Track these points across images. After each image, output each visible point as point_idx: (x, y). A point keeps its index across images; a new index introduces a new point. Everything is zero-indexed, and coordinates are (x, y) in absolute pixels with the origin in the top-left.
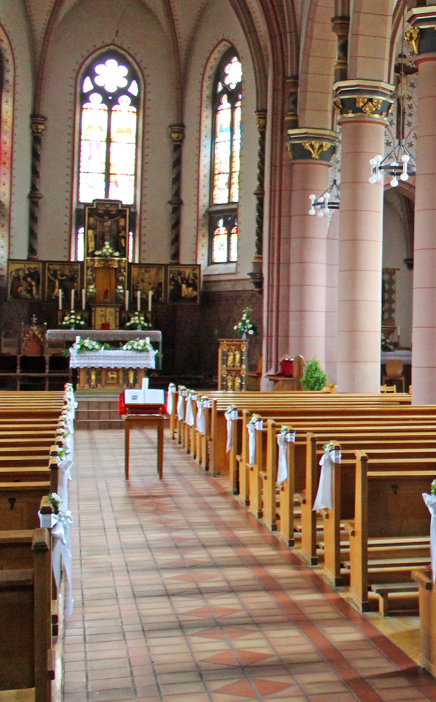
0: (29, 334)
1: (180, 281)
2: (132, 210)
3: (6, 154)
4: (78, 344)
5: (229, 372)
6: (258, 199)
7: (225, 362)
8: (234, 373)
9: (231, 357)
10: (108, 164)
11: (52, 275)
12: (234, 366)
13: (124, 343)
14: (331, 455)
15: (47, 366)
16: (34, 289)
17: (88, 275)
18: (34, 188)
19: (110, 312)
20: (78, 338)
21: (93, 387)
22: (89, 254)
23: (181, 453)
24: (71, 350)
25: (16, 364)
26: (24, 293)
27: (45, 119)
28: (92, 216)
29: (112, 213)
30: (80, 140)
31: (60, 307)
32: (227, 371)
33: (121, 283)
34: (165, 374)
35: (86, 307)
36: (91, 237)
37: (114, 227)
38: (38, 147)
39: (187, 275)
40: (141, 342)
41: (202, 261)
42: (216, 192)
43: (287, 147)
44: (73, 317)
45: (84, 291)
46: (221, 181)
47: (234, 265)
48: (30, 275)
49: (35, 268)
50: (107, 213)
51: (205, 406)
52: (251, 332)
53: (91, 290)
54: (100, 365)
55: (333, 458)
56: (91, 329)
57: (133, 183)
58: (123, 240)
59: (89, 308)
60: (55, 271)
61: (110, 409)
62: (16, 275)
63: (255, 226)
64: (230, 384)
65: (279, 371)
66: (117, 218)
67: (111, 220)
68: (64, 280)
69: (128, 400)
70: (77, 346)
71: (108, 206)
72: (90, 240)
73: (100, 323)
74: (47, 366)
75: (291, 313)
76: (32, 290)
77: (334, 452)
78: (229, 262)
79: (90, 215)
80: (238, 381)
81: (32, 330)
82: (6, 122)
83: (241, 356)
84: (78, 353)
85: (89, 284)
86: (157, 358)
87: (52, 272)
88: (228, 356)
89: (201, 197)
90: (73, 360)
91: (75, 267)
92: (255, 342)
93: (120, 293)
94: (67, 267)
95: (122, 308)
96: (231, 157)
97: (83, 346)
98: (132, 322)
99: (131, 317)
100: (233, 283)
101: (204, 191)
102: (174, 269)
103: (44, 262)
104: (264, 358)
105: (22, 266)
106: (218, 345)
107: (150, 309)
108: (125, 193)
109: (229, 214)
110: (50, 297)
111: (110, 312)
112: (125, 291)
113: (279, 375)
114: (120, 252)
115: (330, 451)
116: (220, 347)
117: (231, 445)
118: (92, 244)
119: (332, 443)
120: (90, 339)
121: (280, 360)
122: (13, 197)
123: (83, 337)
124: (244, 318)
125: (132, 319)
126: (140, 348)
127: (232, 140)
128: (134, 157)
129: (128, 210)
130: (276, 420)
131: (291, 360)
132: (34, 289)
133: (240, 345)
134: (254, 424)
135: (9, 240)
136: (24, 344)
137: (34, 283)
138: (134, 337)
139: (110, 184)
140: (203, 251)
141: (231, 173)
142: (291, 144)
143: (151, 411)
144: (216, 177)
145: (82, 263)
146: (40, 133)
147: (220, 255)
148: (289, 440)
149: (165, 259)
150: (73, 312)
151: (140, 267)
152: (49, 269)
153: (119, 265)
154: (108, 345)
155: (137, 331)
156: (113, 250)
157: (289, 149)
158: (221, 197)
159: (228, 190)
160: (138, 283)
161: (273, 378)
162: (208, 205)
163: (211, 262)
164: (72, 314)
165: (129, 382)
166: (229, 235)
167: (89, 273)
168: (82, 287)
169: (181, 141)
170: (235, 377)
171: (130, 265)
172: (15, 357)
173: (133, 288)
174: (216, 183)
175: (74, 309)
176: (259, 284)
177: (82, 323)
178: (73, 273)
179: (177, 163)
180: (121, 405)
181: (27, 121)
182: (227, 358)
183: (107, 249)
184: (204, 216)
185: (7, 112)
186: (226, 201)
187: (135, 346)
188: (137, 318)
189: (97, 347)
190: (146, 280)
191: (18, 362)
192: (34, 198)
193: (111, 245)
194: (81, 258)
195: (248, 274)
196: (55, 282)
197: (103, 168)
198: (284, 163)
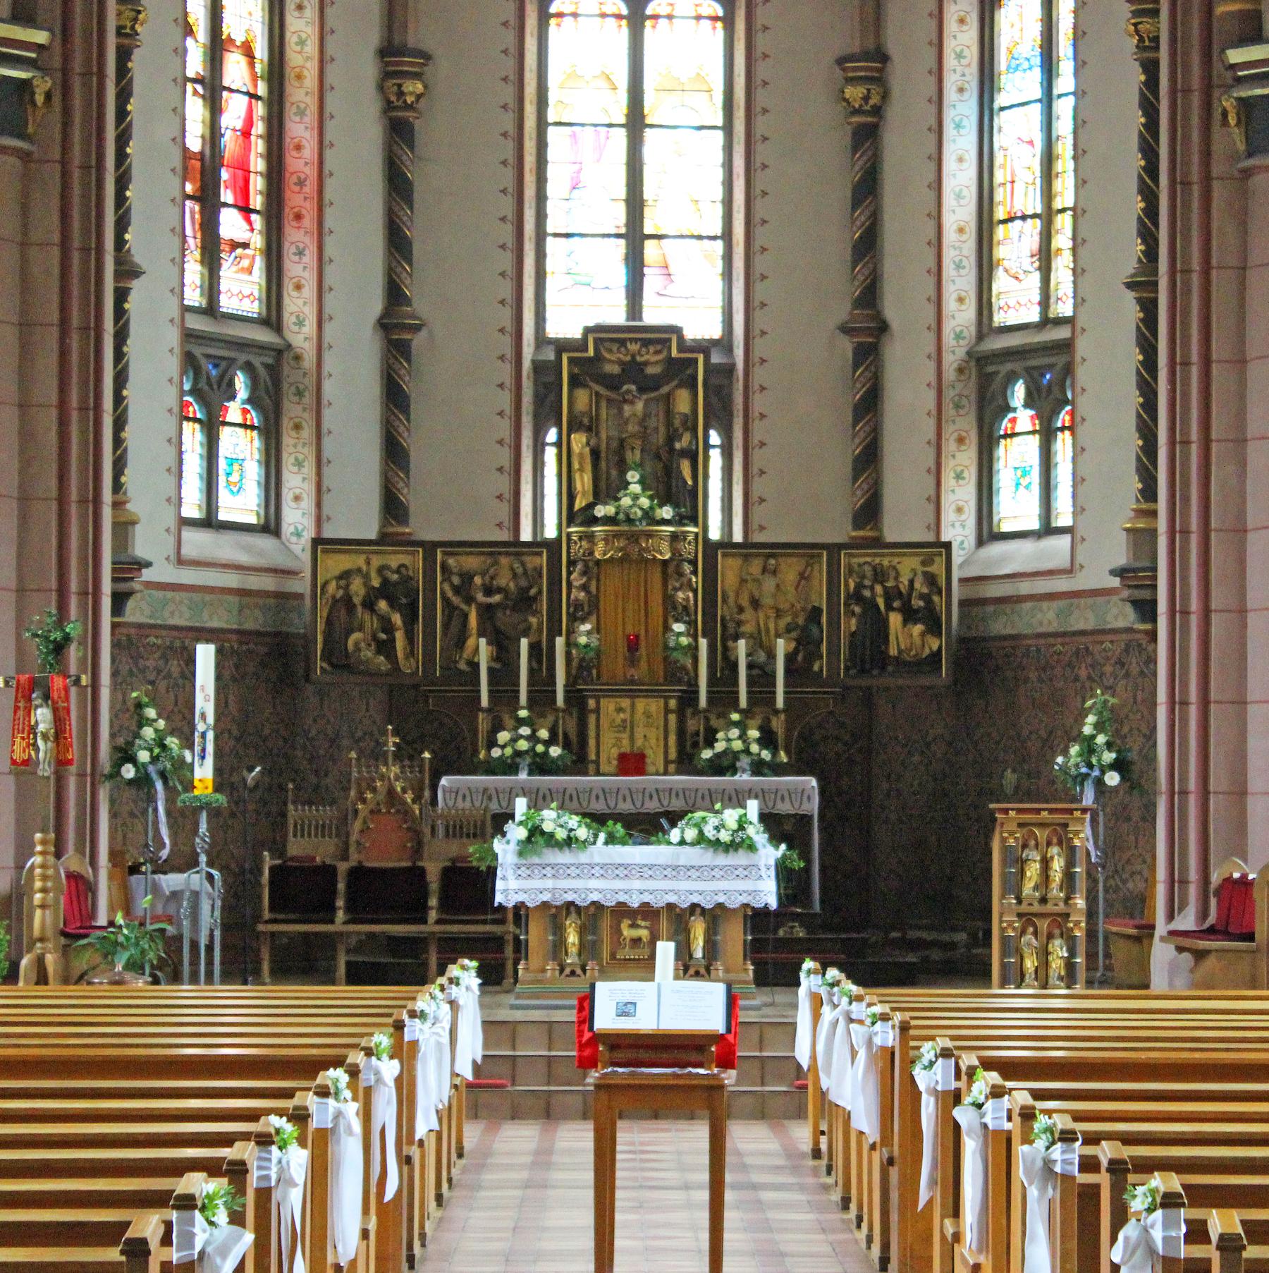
0: (374, 790)
1: (881, 602)
2: (716, 358)
3: (301, 183)
4: (521, 823)
5: (1027, 919)
6: (1139, 301)
7: (1014, 885)
8: (1043, 925)
9: (1036, 867)
10: (635, 203)
11: (457, 590)
12: (1043, 900)
13: (674, 818)
14: (1152, 1226)
15: (433, 902)
16: (399, 636)
17: (574, 586)
18: (395, 294)
19: (648, 715)
20: (521, 805)
21: (573, 973)
22: (570, 515)
23: (820, 1208)
24: (498, 845)
25: (334, 893)
26: (367, 653)
27: (427, 57)
28: (585, 386)
29: (650, 370)
30: (542, 124)
31: (485, 702)
32: (1020, 915)
33: (684, 614)
34: (826, 927)
35: (567, 699)
36: (581, 455)
37: (657, 421)
38: (406, 155)
39: (905, 580)
40: (731, 816)
41: (958, 529)
42: (1001, 283)
43: (1225, 114)
44: (525, 731)
45: (560, 642)
46: (1016, 246)
47: (1065, 540)
48: (386, 591)
49: (403, 565)
50: (633, 370)
51: (878, 1041)
52: (1112, 779)
53: (583, 640)
54: (595, 897)
55: (1158, 1235)
56: (585, 774)
57: (719, 265)
58: (685, 467)
59: (576, 698)
60: (467, 577)
61: (514, 1049)
62: (340, 593)
63: (1135, 399)
64: (1030, 964)
65: (1212, 919)
66: (665, 390)
67: (645, 397)
68: (498, 605)
69: (605, 1019)
70: (517, 832)
71: (633, 347)
72: (576, 466)
73: (615, 752)
74: (433, 902)
75: (1251, 709)
76: (392, 640)
77: (1159, 1213)
78: (1048, 529)
79: (575, 382)
80: (1059, 950)
81: (382, 778)
82: (299, 77)
83: (1070, 863)
84: (520, 854)
85: (573, 618)
86: (784, 872)
87: (456, 580)
88: (1022, 863)
89: (950, 304)
90: (504, 878)
91: (532, 562)
92: (1127, 817)
93: (678, 647)
94: (504, 561)
95: (688, 698)
96: (1049, 159)
97: (536, 832)
98: (720, 746)
99: (716, 731)
100: (1062, 603)
101: (959, 281)
102: (862, 559)
103: (430, 548)
104: (1161, 873)
105: (360, 561)
106: (988, 825)
107: (780, 703)
108: (692, 299)
109: (1046, 361)
110: (449, 665)
111: (648, 715)
112: (696, 640)
113: (1211, 932)
114: (676, 505)
115: (1150, 1210)
116: (998, 829)
117: (933, 1183)
118: (584, 482)
119: (1159, 1182)
120: (561, 807)
121: (1216, 878)
122: (328, 328)
123: (537, 803)
124: (1087, 730)
125: (720, 735)
126: (725, 836)
127: (1048, 99)
128: (719, 174)
129: (701, 358)
130: (1038, 1095)
131: (1251, 877)
132: (399, 636)
133: (1066, 825)
134: (980, 1106)
135: (319, 474)
136: (357, 825)
137: (397, 619)
138: (709, 801)
139: (646, 270)
140: (960, 495)
141: (1047, 217)
142: (1239, 99)
143: (684, 1056)
144: (1000, 232)
145: (553, 547)
146: (410, 107)
147: (1017, 507)
148: (1058, 1169)
149: (838, 530)
150: (523, 713)
151: (746, 557)
152: (445, 568)
153: (675, 552)
154: (619, 829)
155: (736, 777)
156: (651, 498)
157: (1232, 120)
158: (1017, 302)
159: (1037, 276)
160: (741, 610)
161: (1187, 942)
162: (973, 329)
163: (987, 533)
164: (521, 722)
165: (691, 956)
166: (1047, 435)
167: (577, 579)
168: (554, 631)
169: (877, 111)
170: (1050, 936)
171: (711, 549)
172: (328, 872)
173: (724, 626)
174: (1000, 252)
175: (530, 707)
176: (1147, 609)
177: (555, 751)
178: (523, 583)
179: (867, 188)
180: (580, 1033)
181: (369, 69)
182: (1022, 872)
183: (635, 495)
184: (960, 370)
185: (302, 43)
186: (1033, 316)
187: (709, 832)
188: (734, 733)
189: (582, 833)
190: (767, 601)
191: (341, 886)
192: (396, 331)
193: (642, 482)
194: (550, 532)
195: (1113, 573)
196: (466, 616)
197: (617, 217)
198: (1216, 170)
